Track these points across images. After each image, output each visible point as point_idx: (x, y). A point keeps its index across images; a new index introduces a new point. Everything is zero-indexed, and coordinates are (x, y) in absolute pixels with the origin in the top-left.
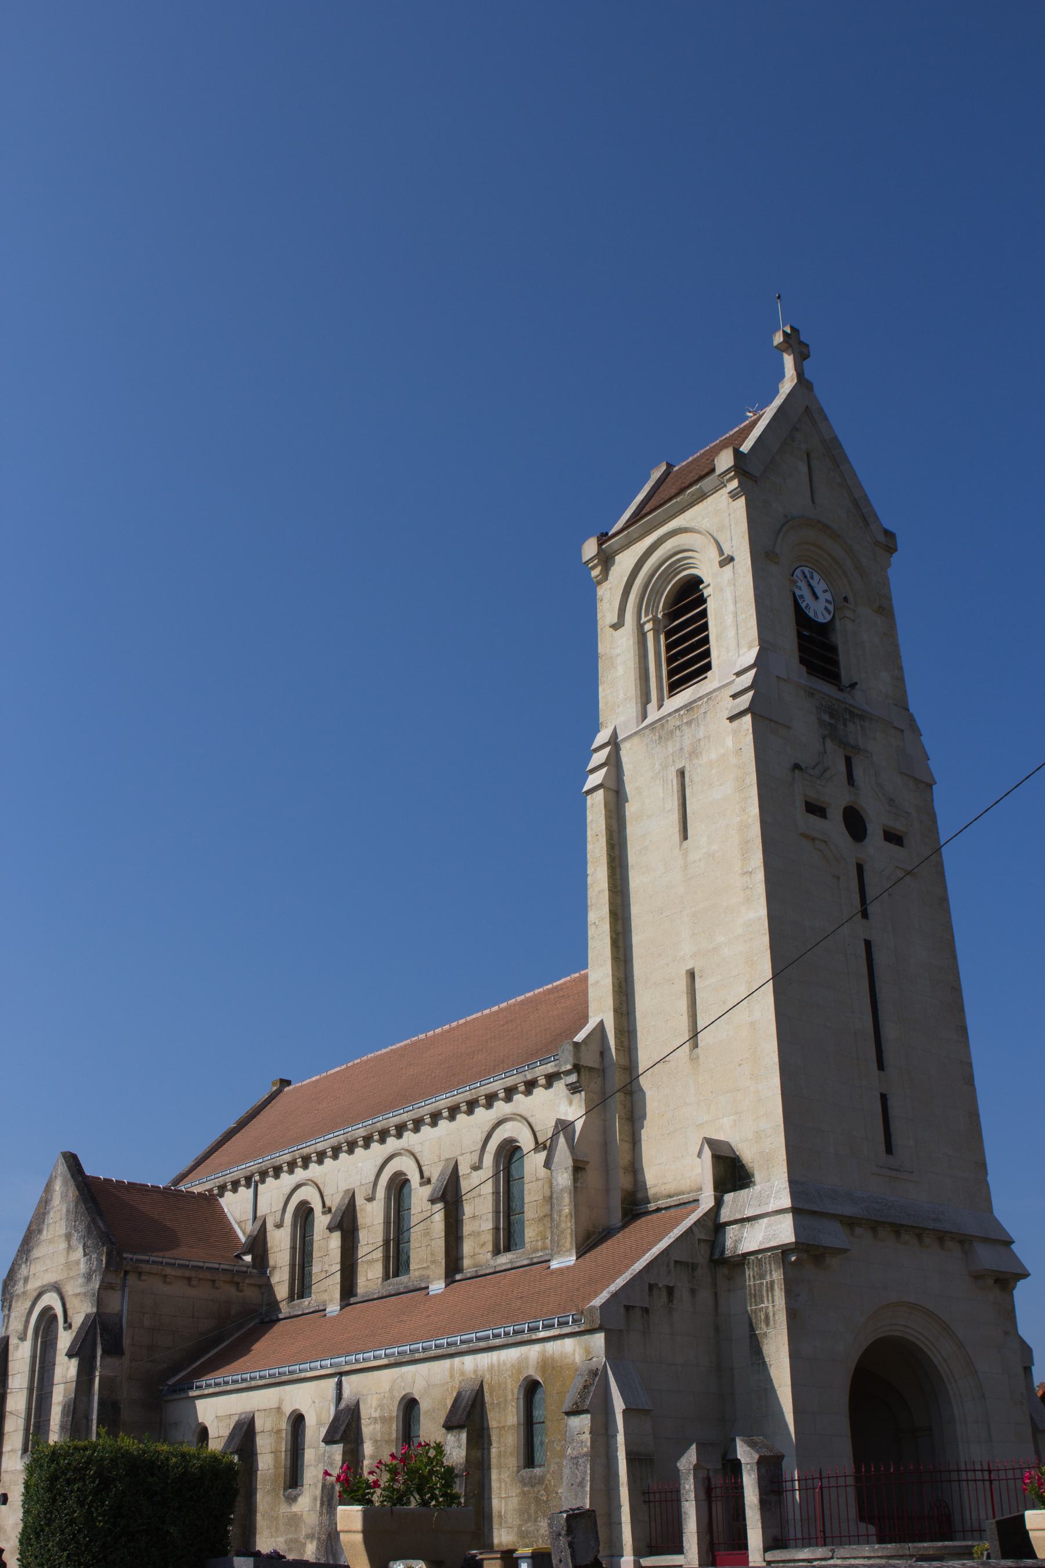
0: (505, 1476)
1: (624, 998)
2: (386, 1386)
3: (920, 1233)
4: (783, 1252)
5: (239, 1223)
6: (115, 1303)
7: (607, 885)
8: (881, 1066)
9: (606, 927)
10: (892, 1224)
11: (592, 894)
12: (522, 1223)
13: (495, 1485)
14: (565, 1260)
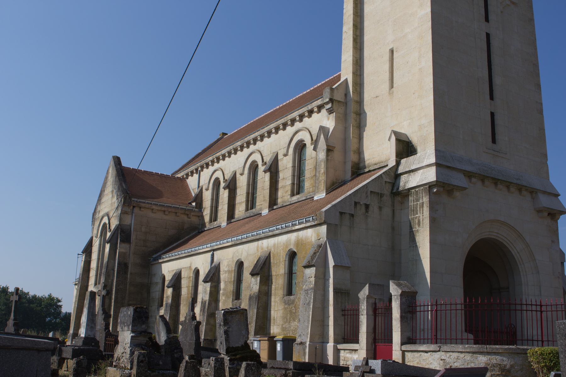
0: (277, 299)
1: (359, 68)
2: (230, 256)
3: (508, 185)
4: (429, 187)
5: (193, 190)
6: (129, 220)
7: (352, 12)
8: (492, 98)
9: (351, 32)
10: (493, 179)
11: (345, 17)
12: (304, 180)
13: (273, 304)
14: (321, 195)
